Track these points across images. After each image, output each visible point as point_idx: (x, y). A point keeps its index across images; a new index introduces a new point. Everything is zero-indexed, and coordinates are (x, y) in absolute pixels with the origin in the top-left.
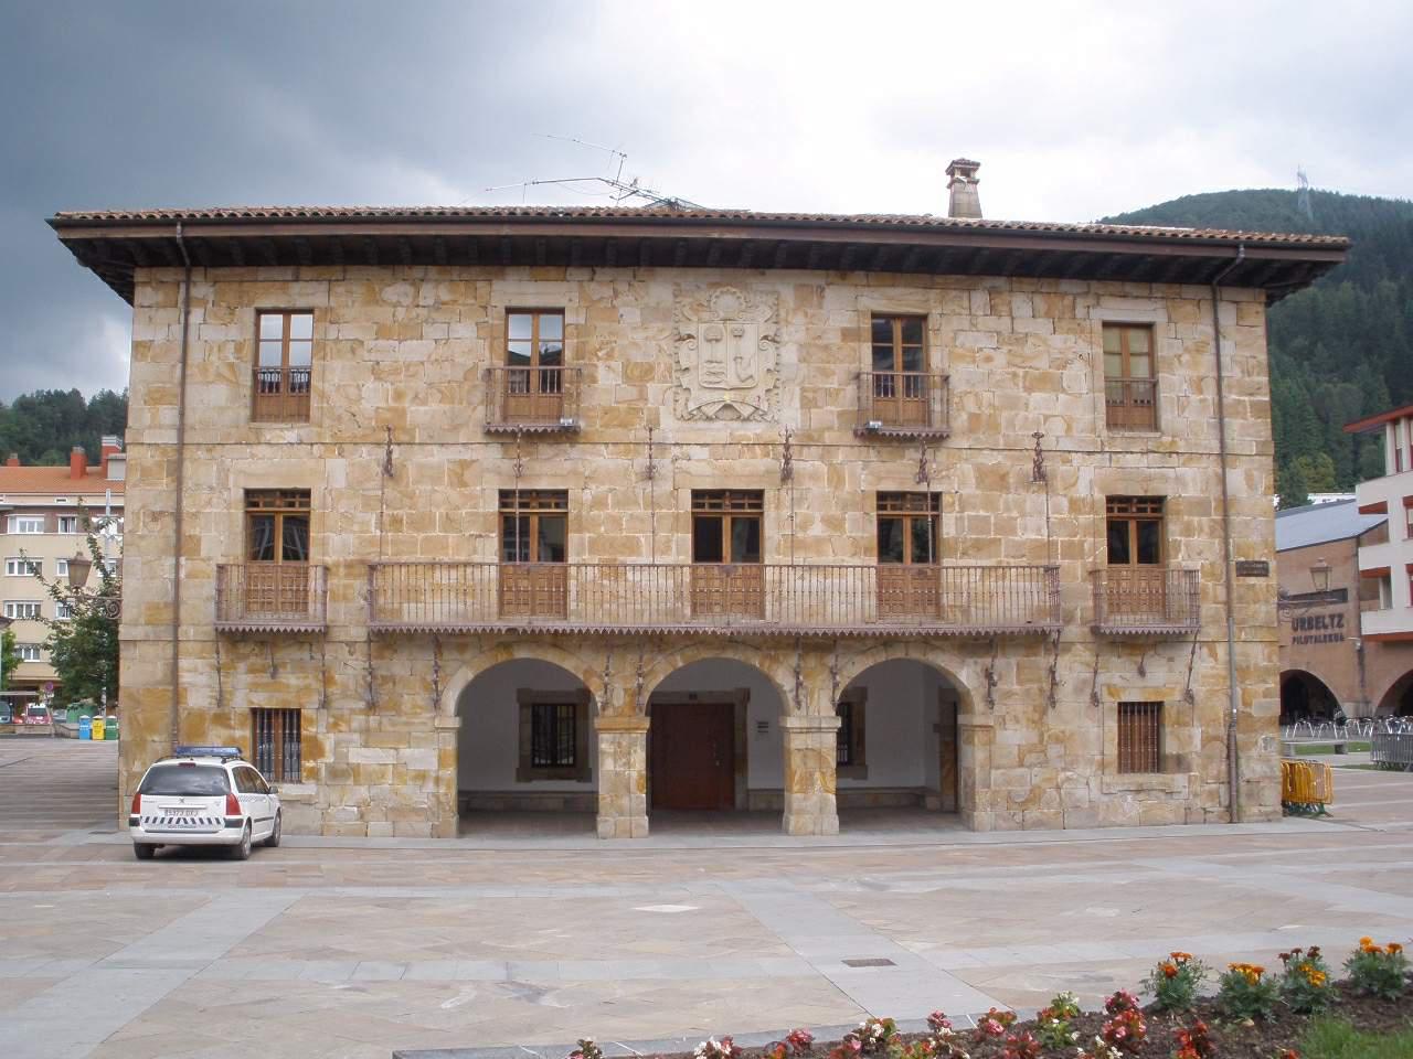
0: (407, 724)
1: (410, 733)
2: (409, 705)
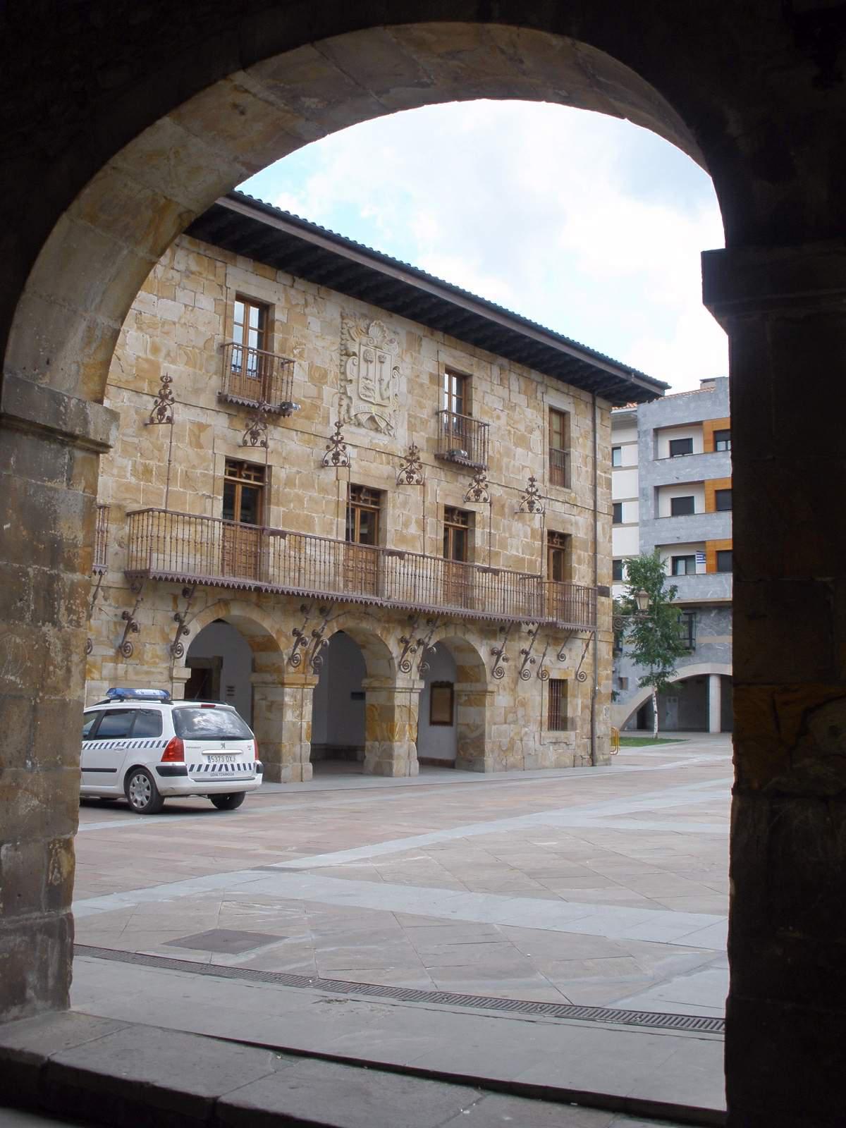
0: (147, 673)
1: (150, 682)
2: (150, 655)
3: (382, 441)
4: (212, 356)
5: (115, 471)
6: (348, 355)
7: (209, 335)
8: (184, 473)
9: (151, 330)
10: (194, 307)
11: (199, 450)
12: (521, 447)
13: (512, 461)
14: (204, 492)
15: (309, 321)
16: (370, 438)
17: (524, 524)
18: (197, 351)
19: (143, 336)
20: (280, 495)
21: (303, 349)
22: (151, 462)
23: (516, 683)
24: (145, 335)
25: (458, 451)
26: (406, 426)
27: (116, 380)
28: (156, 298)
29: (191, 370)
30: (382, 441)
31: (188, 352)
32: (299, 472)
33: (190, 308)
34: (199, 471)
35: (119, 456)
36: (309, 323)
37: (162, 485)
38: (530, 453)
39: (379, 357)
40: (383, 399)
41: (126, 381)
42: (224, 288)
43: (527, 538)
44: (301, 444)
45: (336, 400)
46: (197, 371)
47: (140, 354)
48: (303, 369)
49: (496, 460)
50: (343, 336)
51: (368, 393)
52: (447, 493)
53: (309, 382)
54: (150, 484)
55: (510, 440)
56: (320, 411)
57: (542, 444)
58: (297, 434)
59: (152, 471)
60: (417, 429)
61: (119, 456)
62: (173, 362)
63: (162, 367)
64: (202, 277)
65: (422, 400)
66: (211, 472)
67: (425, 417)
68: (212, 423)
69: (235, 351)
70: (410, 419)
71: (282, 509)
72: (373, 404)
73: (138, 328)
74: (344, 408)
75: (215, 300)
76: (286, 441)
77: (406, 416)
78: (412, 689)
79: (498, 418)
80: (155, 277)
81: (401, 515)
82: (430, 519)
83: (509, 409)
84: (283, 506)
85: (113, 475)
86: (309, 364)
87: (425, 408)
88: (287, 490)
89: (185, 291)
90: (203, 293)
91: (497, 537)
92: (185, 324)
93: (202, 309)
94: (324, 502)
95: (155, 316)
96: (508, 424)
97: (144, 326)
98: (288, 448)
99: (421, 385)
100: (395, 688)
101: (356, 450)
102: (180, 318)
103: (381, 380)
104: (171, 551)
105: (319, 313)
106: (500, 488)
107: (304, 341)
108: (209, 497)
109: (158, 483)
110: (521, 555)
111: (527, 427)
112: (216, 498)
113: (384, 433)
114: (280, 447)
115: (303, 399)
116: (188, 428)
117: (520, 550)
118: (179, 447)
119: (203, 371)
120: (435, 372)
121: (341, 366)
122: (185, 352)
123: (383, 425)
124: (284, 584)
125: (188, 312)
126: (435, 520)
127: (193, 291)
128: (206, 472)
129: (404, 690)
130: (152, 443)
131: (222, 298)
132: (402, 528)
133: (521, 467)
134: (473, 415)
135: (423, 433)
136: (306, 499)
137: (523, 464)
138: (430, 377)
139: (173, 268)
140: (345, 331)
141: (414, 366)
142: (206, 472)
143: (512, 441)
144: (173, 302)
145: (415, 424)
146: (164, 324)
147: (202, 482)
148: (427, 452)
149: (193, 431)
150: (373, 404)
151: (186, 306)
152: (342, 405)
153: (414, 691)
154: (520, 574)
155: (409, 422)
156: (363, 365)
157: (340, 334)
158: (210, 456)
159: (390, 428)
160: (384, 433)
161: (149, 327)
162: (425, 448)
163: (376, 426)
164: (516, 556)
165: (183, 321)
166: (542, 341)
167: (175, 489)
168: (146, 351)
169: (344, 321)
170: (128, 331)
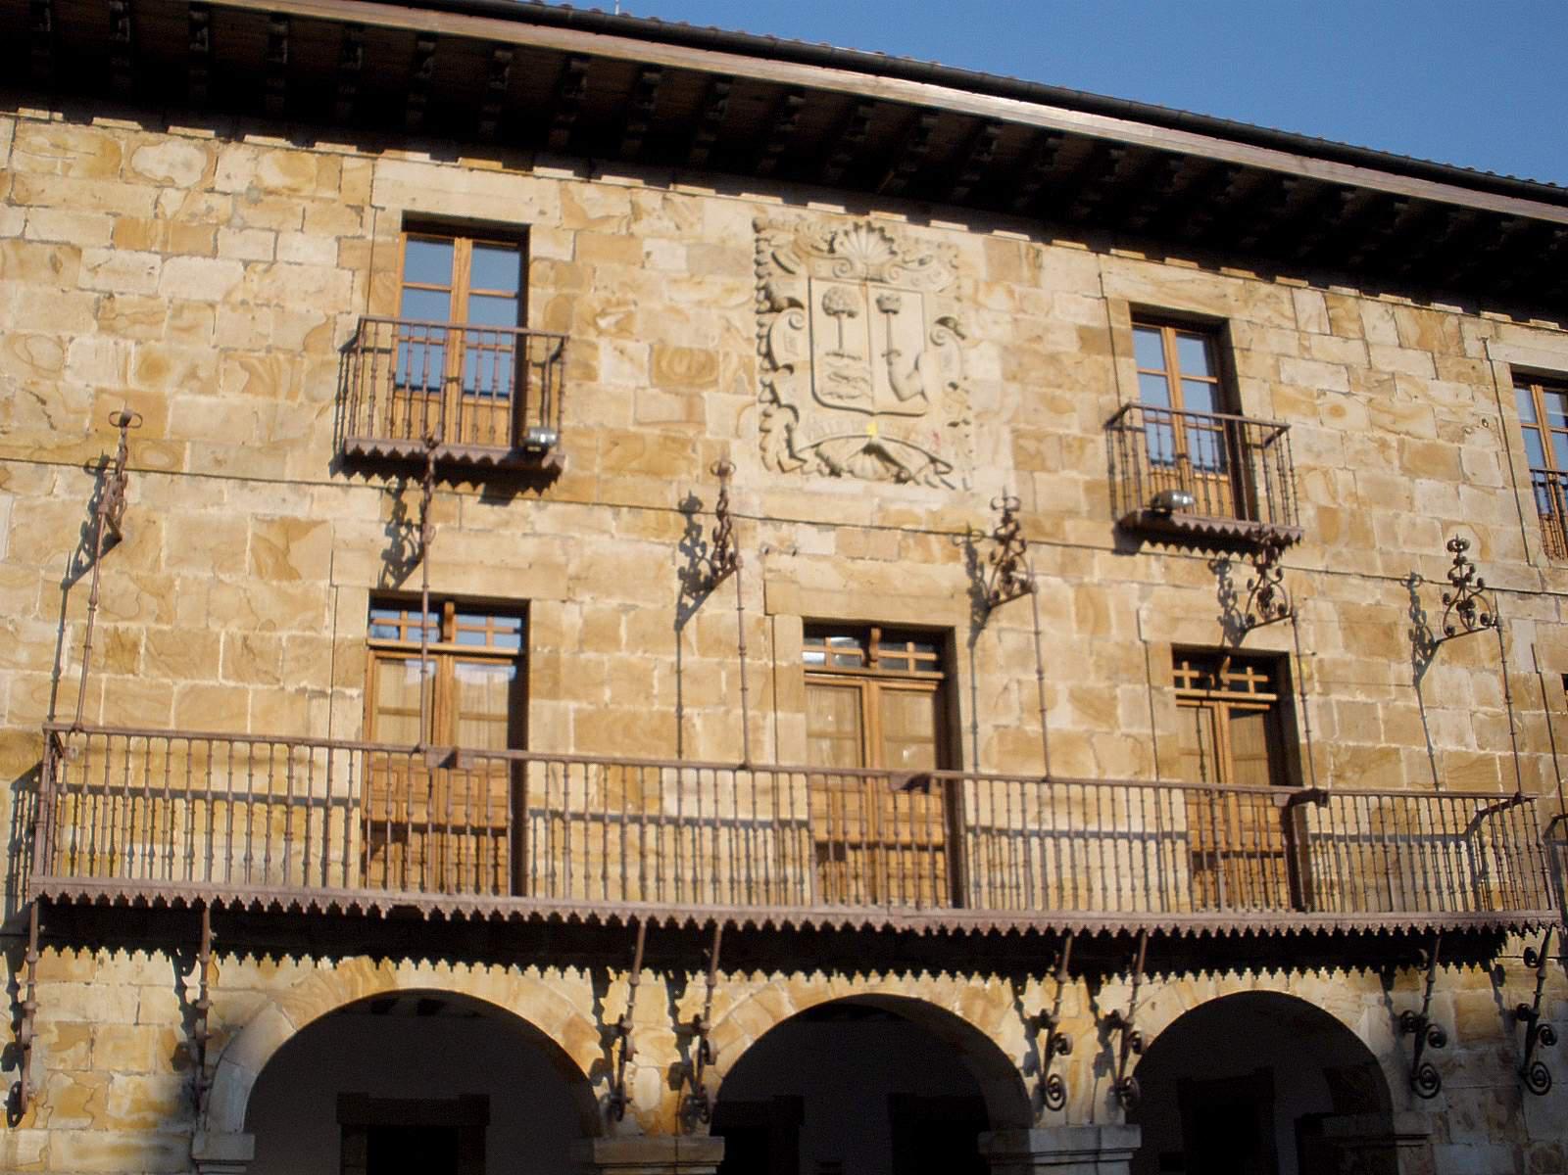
3: (923, 501)
4: (325, 364)
5: (23, 656)
6: (775, 309)
7: (318, 317)
8: (239, 643)
9: (138, 328)
10: (275, 261)
11: (285, 584)
12: (1431, 475)
13: (1405, 516)
14: (303, 684)
15: (646, 249)
16: (876, 501)
17: (1474, 665)
18: (281, 356)
19: (116, 343)
20: (563, 670)
21: (629, 316)
22: (134, 626)
23: (1516, 1104)
24: (120, 340)
25: (1205, 508)
26: (1006, 459)
27: (27, 447)
28: (158, 258)
29: (261, 402)
30: (923, 501)
31: (256, 363)
32: (626, 609)
33: (261, 267)
34: (284, 635)
35: (37, 618)
36: (648, 254)
37: (166, 676)
38: (1463, 489)
39: (879, 302)
40: (901, 399)
41: (58, 447)
42: (369, 212)
43: (1491, 704)
44: (634, 536)
45: (752, 418)
46: (281, 400)
47: (105, 384)
48: (631, 360)
49: (1344, 517)
50: (762, 271)
51: (844, 389)
52: (1178, 613)
53: (653, 385)
54: (131, 676)
55: (1389, 462)
56: (694, 450)
57: (1505, 463)
58: (617, 516)
59: (136, 645)
60: (1051, 464)
61: (37, 618)
62: (209, 388)
63: (170, 404)
64: (300, 197)
65: (1058, 392)
66: (328, 634)
67: (1075, 431)
68: (328, 516)
69: (1192, 433)
70: (1022, 442)
71: (571, 705)
72: (871, 414)
73: (101, 329)
74: (778, 433)
75: (339, 239)
76: (577, 535)
77: (1006, 435)
78: (1097, 1152)
79: (1337, 412)
80: (156, 216)
81: (1014, 686)
82: (1126, 686)
83: (1369, 390)
84: (575, 697)
85: (16, 665)
86: (651, 346)
87: (1073, 410)
88: (589, 655)
89: (245, 232)
90: (302, 230)
91: (1380, 713)
92: (244, 303)
93: (300, 264)
94: (724, 675)
95: (154, 297)
96: (1373, 424)
97: (121, 323)
98: (588, 551)
99: (1053, 359)
100: (1031, 1155)
101: (832, 535)
102: (229, 294)
103: (890, 355)
104: (1098, 799)
105: (678, 228)
106: (1370, 584)
107: (631, 296)
108: (322, 694)
109: (155, 673)
110: (1475, 750)
111: (1441, 426)
112: (343, 696)
113: (929, 483)
114: (559, 552)
115: (632, 429)
116: (249, 535)
117: (1472, 739)
118: (221, 581)
119: (301, 398)
120: (1099, 324)
121: (760, 337)
122: (242, 365)
123: (914, 462)
124: (643, 898)
125: (255, 278)
126: (1141, 689)
127: (270, 230)
128: (308, 633)
129: (1066, 1159)
130: (136, 580)
131: (359, 232)
132: (1020, 719)
133: (1438, 525)
134: (1244, 412)
135: (1074, 474)
136: (656, 673)
137: (1445, 517)
138: (1081, 338)
139: (212, 190)
140: (767, 258)
141: (1020, 316)
142: (308, 633)
143: (1396, 463)
144: (209, 261)
145: (1039, 452)
146: (179, 311)
147: (297, 659)
148: (1091, 516)
149: (266, 540)
150: (871, 414)
151: (246, 264)
152: (767, 431)
153: (1104, 1157)
154: (1475, 797)
155: (1018, 449)
156: (824, 324)
157: (755, 267)
158: (323, 596)
159: (942, 468)
160: (929, 483)
161: (135, 322)
162: (1084, 508)
163: (894, 470)
164: (1457, 754)
165: (238, 296)
166: (1024, 103)
167: (212, 683)
168: (124, 377)
169: (763, 235)
170: (72, 339)
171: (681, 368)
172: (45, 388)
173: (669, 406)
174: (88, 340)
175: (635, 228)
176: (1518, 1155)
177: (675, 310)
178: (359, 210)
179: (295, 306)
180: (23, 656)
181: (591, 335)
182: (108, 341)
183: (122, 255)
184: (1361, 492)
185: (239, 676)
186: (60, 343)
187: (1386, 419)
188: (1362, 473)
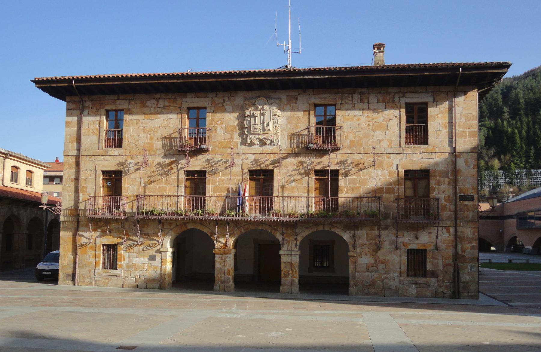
38: (387, 132)
106: (360, 155)
151: (164, 120)
171: (230, 129)
172: (137, 143)
173: (228, 136)
174: (142, 135)
175: (224, 104)
176: (376, 260)
177: (230, 119)
178: (180, 108)
179: (172, 126)
180: (137, 184)
181: (217, 125)
182: (145, 135)
183: (146, 120)
184: (361, 136)
185: (166, 184)
186: (139, 136)
187: (370, 119)
188: (362, 132)
